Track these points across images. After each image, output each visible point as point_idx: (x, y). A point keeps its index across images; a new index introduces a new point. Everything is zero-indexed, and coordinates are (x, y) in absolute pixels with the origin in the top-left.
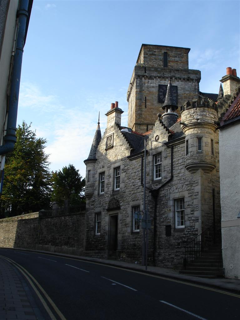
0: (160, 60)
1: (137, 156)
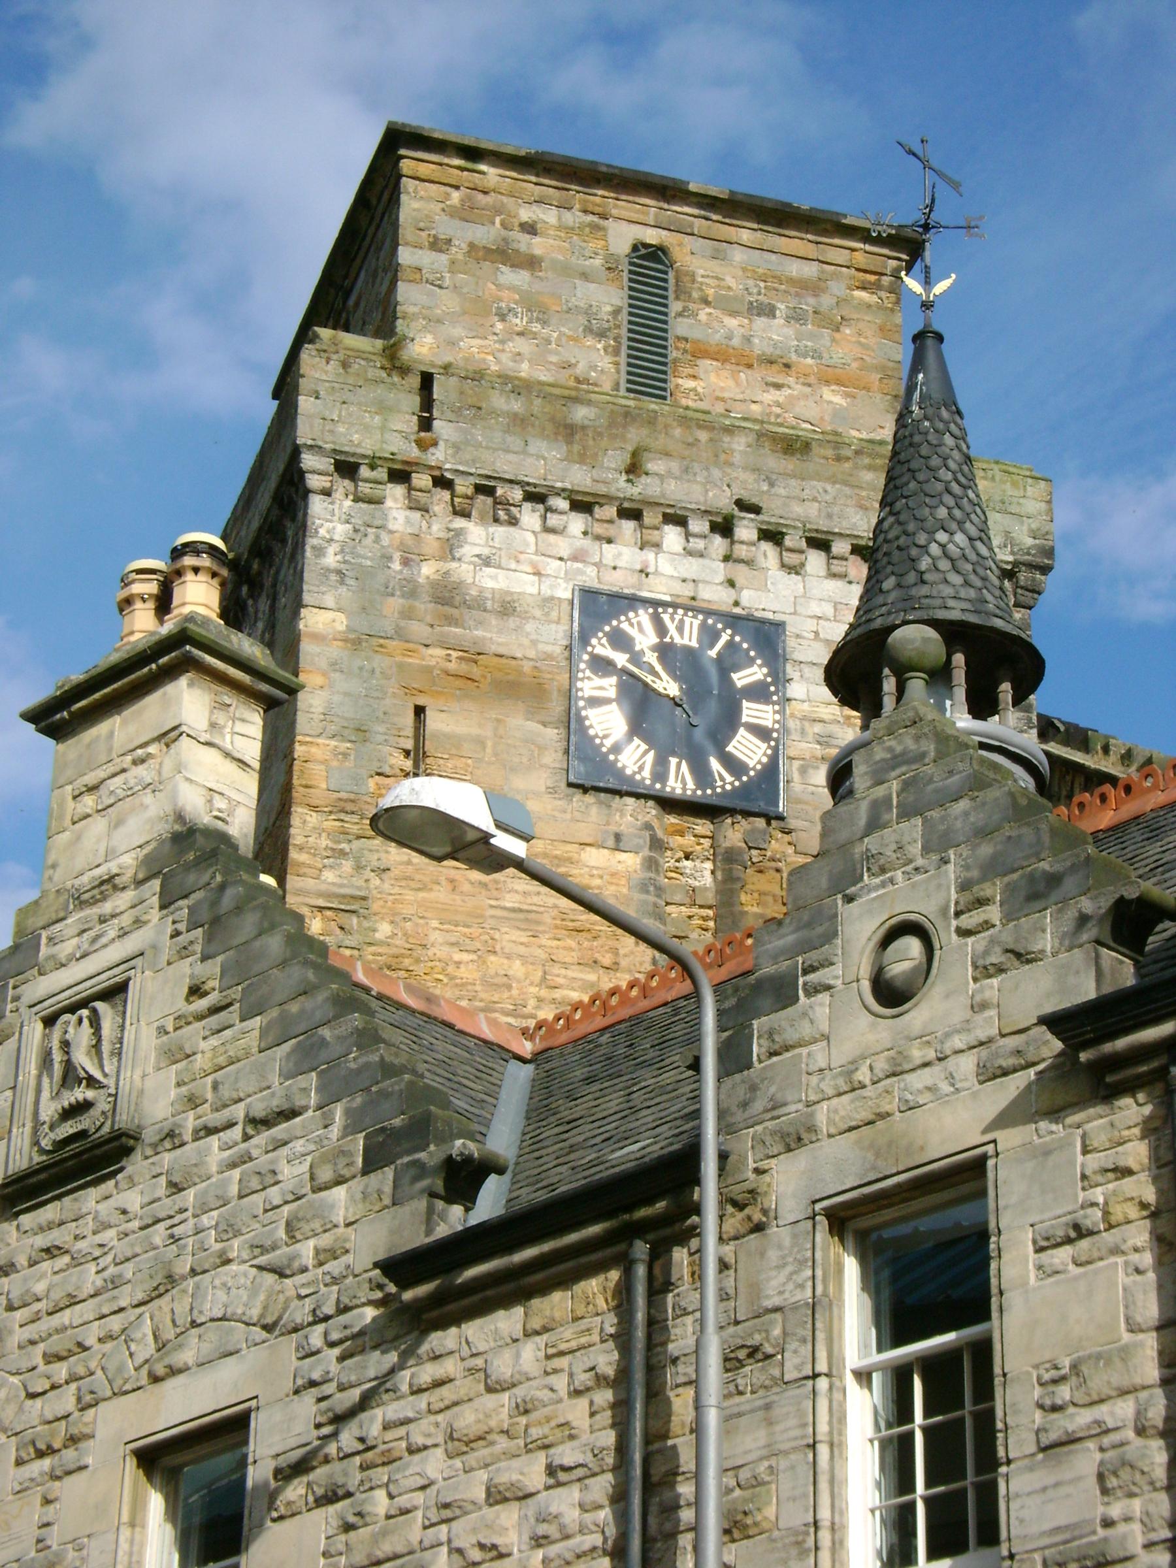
0: (588, 330)
1: (547, 1247)
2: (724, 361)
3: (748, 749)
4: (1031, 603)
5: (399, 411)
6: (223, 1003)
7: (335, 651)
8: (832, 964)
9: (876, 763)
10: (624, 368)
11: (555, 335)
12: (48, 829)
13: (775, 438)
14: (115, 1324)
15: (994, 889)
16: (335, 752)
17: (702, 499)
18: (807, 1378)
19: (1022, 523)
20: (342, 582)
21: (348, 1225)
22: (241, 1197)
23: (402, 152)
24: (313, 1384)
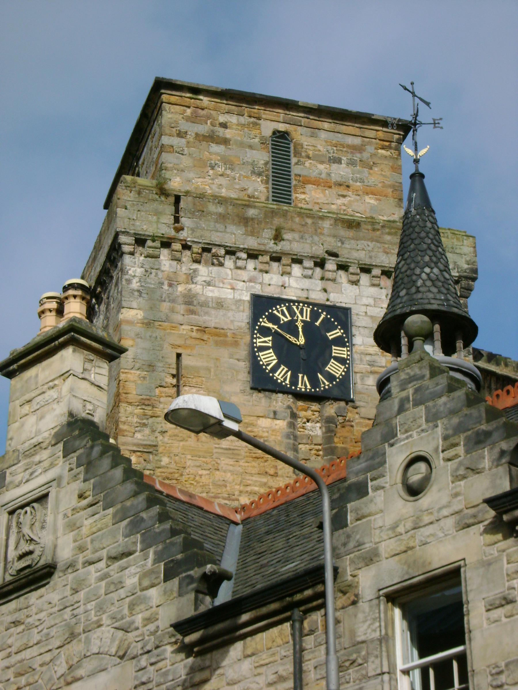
0: (253, 172)
2: (318, 185)
3: (335, 368)
4: (467, 295)
5: (165, 214)
6: (94, 502)
7: (138, 328)
8: (384, 476)
9: (401, 380)
10: (271, 190)
11: (238, 175)
12: (8, 421)
13: (343, 221)
14: (47, 657)
15: (461, 439)
16: (139, 377)
17: (310, 251)
18: (379, 674)
19: (462, 258)
20: (140, 296)
21: (157, 607)
22: (106, 595)
23: (163, 91)
24: (144, 683)
